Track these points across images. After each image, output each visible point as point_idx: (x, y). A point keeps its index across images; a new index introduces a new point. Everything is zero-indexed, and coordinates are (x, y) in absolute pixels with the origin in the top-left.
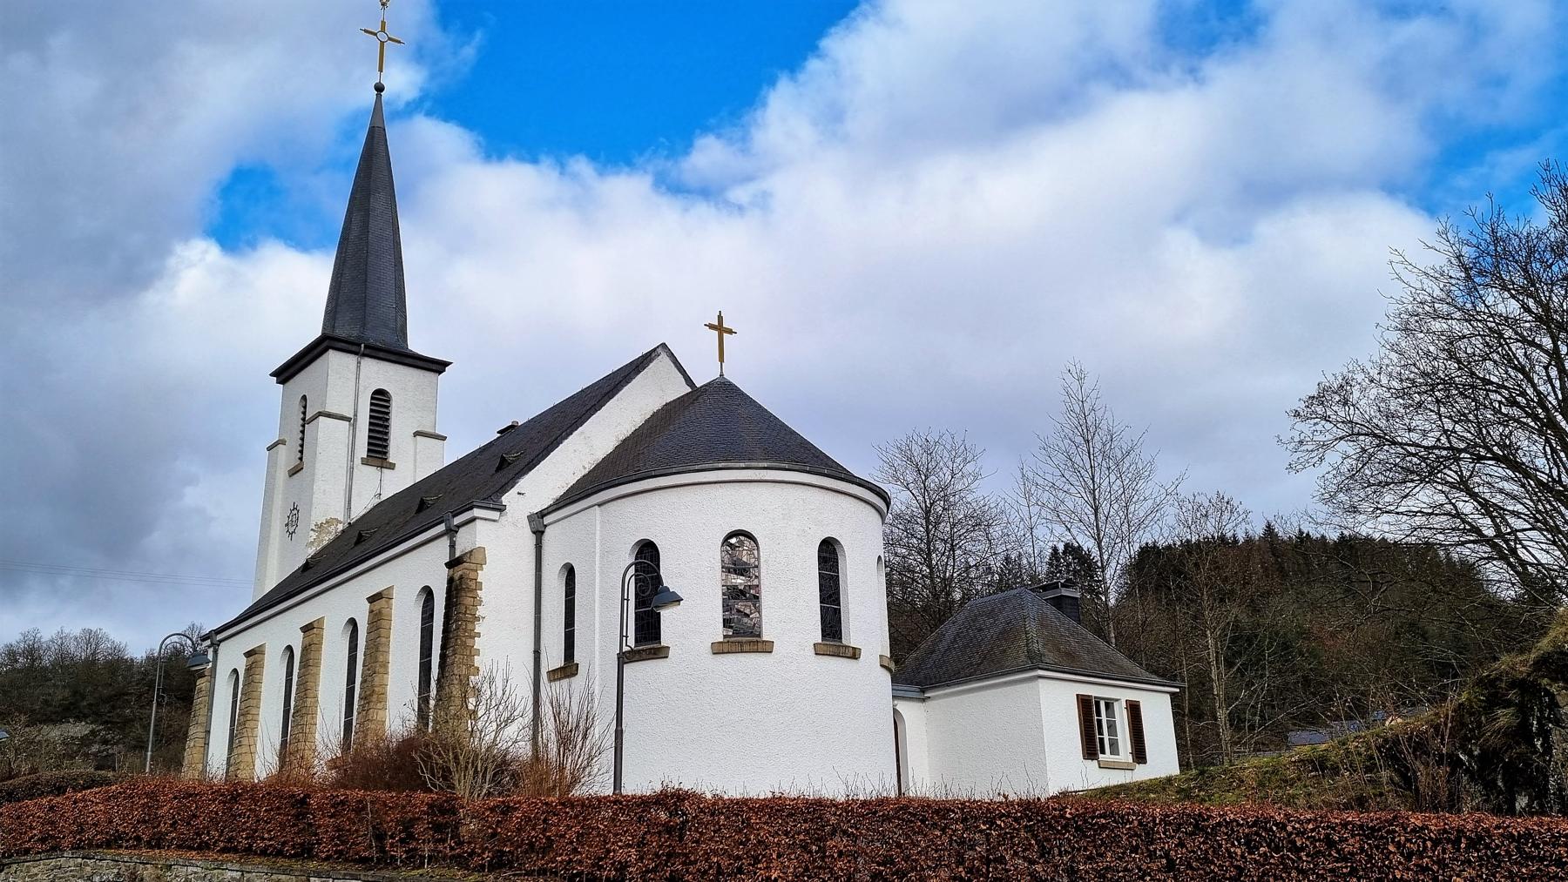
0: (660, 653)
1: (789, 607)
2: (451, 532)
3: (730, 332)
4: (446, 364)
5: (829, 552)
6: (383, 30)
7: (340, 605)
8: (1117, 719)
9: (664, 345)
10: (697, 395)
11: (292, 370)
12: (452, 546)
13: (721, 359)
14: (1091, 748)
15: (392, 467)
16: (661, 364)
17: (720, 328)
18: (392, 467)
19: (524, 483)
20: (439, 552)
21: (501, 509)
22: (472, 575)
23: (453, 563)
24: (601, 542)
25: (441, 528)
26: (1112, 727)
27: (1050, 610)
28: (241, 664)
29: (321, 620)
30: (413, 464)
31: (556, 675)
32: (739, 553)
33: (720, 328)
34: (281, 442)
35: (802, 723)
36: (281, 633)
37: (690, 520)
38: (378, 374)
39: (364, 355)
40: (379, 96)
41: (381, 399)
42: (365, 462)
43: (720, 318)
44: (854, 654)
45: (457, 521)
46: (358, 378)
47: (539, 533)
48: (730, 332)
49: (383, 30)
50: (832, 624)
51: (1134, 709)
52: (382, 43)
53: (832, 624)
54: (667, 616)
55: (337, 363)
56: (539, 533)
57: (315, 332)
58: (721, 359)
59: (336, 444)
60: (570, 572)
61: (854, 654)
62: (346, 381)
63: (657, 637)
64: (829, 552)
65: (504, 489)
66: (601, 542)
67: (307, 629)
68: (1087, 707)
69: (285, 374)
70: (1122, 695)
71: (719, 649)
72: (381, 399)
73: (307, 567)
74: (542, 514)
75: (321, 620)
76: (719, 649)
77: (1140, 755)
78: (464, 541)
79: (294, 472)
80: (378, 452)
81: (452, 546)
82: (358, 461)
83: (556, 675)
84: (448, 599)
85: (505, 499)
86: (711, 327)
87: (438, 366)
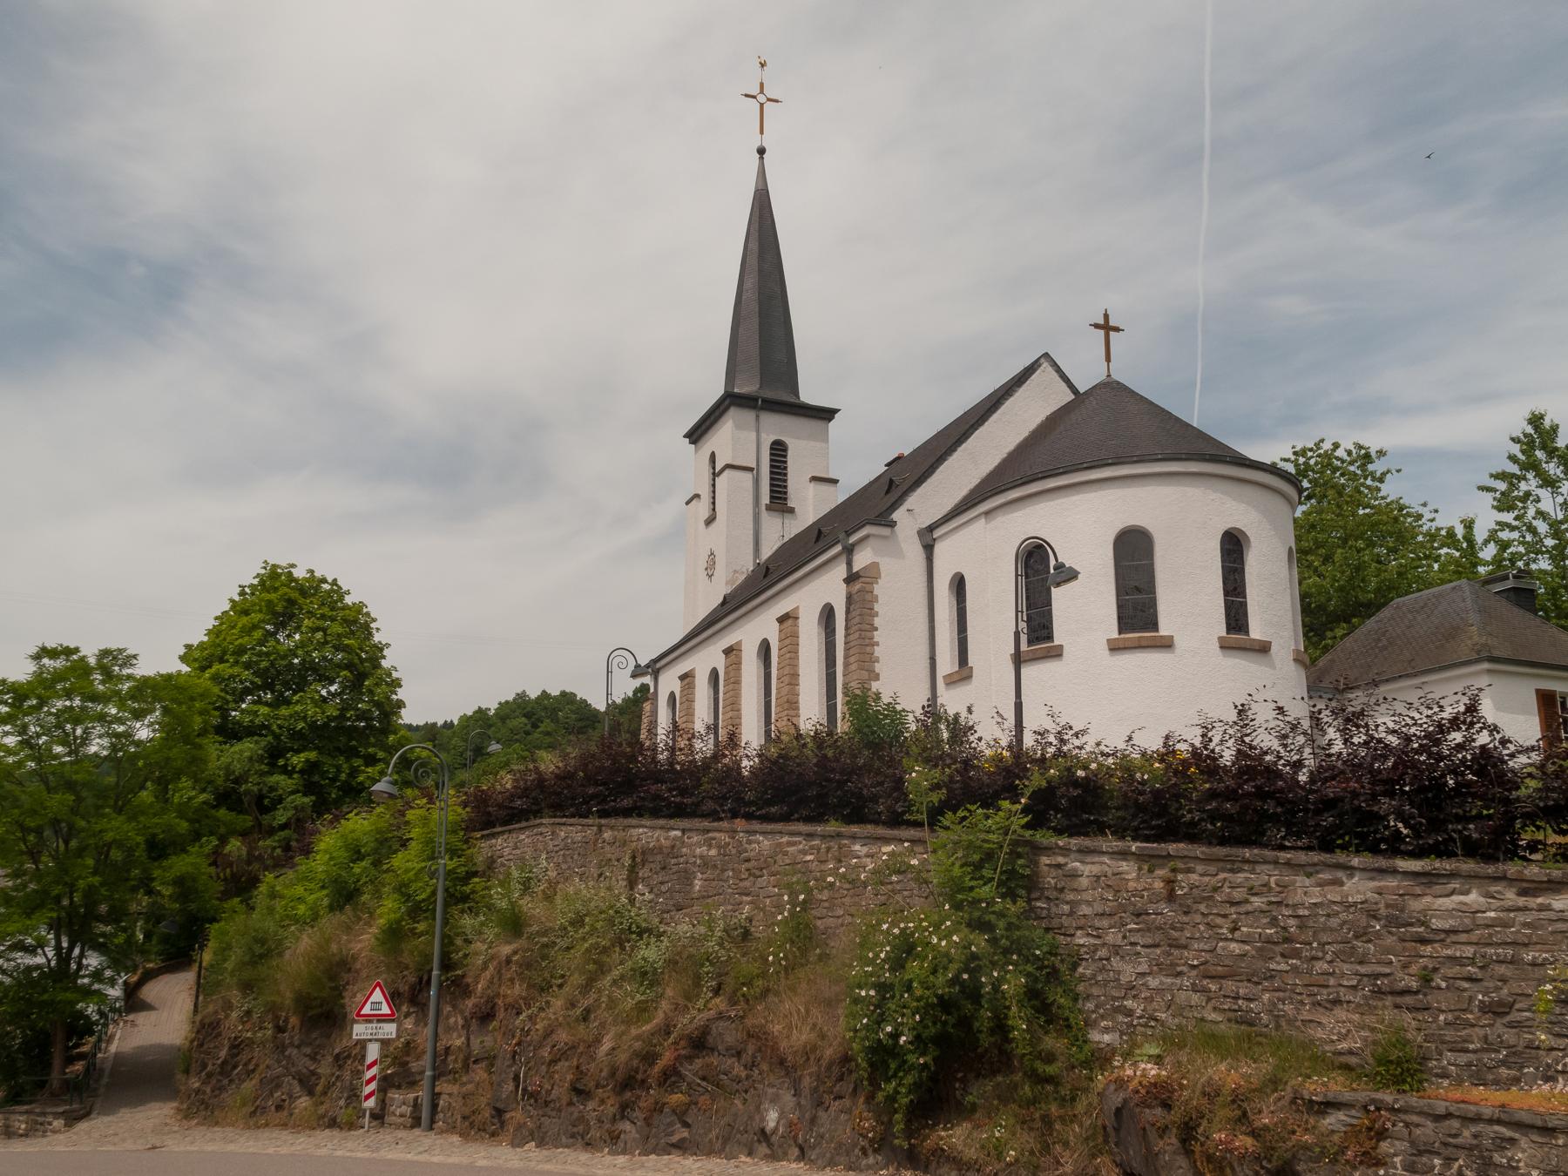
0: (1057, 653)
1: (1188, 596)
2: (849, 551)
3: (1117, 329)
4: (836, 411)
5: (1233, 546)
6: (762, 92)
7: (759, 628)
9: (1046, 355)
12: (849, 564)
13: (1108, 359)
15: (792, 511)
16: (1045, 373)
17: (1107, 327)
19: (912, 501)
20: (840, 571)
21: (892, 524)
22: (868, 587)
23: (851, 579)
24: (986, 553)
25: (838, 548)
28: (676, 687)
29: (739, 643)
30: (810, 505)
31: (952, 681)
33: (1107, 327)
36: (708, 659)
37: (1078, 525)
38: (775, 427)
39: (762, 409)
40: (762, 158)
42: (768, 508)
43: (1106, 316)
45: (852, 539)
47: (929, 549)
48: (1117, 329)
49: (762, 92)
50: (1236, 619)
52: (762, 105)
53: (1236, 619)
54: (1059, 595)
56: (929, 549)
57: (718, 390)
58: (1108, 359)
60: (959, 585)
61: (1263, 648)
63: (1050, 638)
65: (894, 506)
66: (986, 553)
71: (1115, 648)
72: (779, 449)
74: (931, 528)
75: (739, 643)
76: (1115, 648)
78: (861, 560)
80: (779, 500)
81: (849, 564)
84: (848, 612)
85: (895, 516)
86: (1097, 326)
87: (827, 414)
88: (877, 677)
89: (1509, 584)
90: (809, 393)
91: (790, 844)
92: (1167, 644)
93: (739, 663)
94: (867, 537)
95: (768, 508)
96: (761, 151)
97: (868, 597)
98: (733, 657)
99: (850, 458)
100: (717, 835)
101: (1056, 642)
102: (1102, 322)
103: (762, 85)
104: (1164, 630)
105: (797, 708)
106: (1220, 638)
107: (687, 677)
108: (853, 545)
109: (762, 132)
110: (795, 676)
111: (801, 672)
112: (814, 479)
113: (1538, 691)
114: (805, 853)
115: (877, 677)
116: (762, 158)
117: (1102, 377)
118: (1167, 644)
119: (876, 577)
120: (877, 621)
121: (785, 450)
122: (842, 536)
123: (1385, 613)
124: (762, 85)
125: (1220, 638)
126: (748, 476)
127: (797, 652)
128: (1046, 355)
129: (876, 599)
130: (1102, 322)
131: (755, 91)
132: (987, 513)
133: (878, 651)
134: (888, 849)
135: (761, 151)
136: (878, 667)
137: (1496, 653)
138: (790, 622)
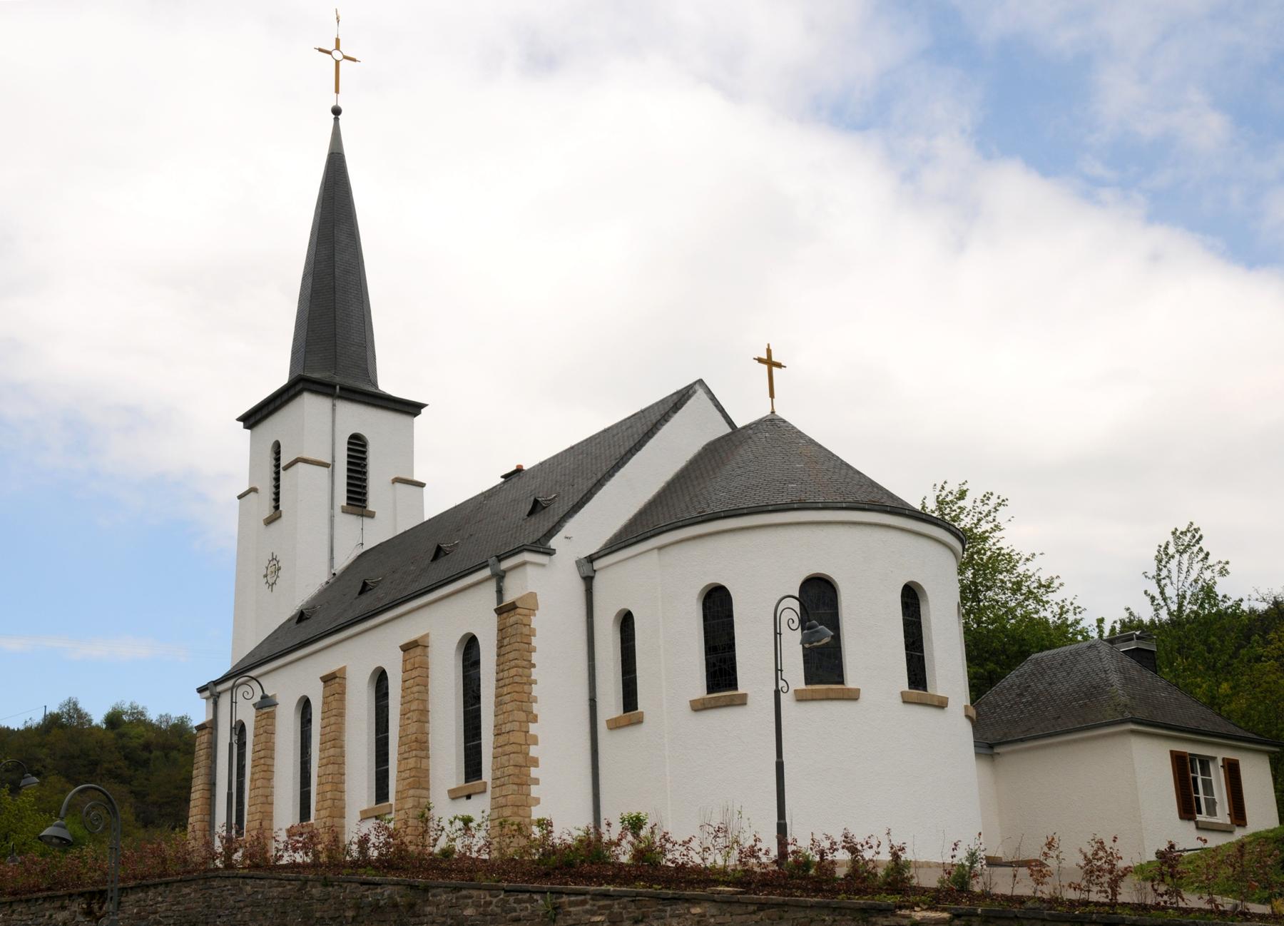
3: (779, 365)
5: (911, 597)
6: (337, 48)
8: (1213, 778)
9: (700, 382)
10: (736, 438)
11: (258, 416)
12: (500, 592)
13: (772, 395)
14: (1188, 808)
15: (371, 515)
16: (699, 401)
17: (770, 363)
18: (371, 515)
19: (570, 527)
21: (550, 552)
22: (525, 621)
23: (503, 610)
24: (662, 590)
25: (486, 572)
26: (1208, 786)
27: (1129, 662)
29: (343, 670)
31: (614, 725)
32: (819, 597)
33: (770, 363)
34: (253, 490)
35: (896, 778)
37: (762, 566)
38: (354, 418)
40: (336, 120)
41: (357, 446)
43: (769, 351)
44: (941, 704)
45: (505, 565)
46: (333, 421)
47: (588, 580)
48: (779, 365)
49: (337, 48)
50: (917, 674)
51: (1232, 770)
52: (337, 63)
53: (917, 674)
55: (311, 406)
56: (588, 580)
57: (280, 377)
58: (772, 395)
59: (315, 491)
61: (941, 704)
62: (319, 424)
64: (911, 597)
66: (662, 590)
67: (327, 679)
68: (1181, 765)
69: (252, 419)
70: (1221, 754)
71: (699, 707)
72: (357, 446)
73: (301, 617)
74: (591, 559)
75: (343, 670)
76: (699, 707)
77: (1238, 814)
79: (269, 521)
80: (357, 498)
81: (500, 592)
82: (338, 510)
83: (614, 725)
85: (554, 543)
87: (412, 409)
88: (535, 719)
89: (1133, 645)
90: (387, 384)
91: (572, 904)
92: (853, 696)
93: (342, 693)
94: (524, 564)
95: (344, 511)
96: (337, 111)
97: (525, 630)
98: (335, 686)
99: (449, 465)
100: (475, 893)
101: (741, 690)
102: (765, 357)
103: (338, 41)
104: (851, 681)
105: (427, 749)
106: (902, 693)
107: (266, 704)
108: (505, 572)
109: (337, 91)
110: (424, 712)
111: (430, 707)
112: (397, 480)
113: (1172, 752)
114: (594, 913)
115: (535, 719)
116: (336, 120)
117: (764, 412)
118: (853, 696)
119: (533, 610)
120: (535, 658)
121: (364, 445)
122: (492, 560)
123: (1026, 667)
124: (338, 41)
125: (902, 693)
126: (325, 470)
127: (426, 685)
128: (700, 382)
129: (532, 633)
130: (765, 357)
131: (331, 47)
132: (660, 548)
133: (536, 691)
134: (697, 910)
135: (337, 111)
136: (536, 708)
137: (1137, 715)
138: (418, 650)
